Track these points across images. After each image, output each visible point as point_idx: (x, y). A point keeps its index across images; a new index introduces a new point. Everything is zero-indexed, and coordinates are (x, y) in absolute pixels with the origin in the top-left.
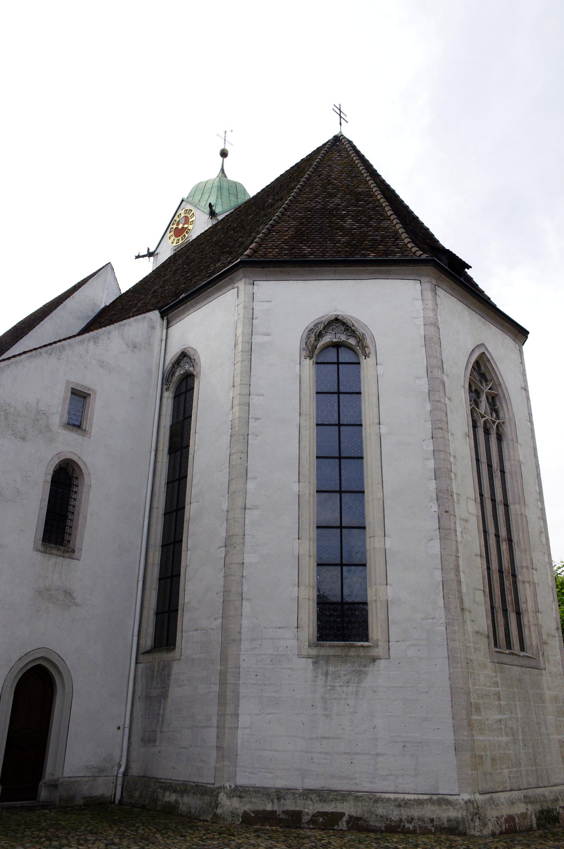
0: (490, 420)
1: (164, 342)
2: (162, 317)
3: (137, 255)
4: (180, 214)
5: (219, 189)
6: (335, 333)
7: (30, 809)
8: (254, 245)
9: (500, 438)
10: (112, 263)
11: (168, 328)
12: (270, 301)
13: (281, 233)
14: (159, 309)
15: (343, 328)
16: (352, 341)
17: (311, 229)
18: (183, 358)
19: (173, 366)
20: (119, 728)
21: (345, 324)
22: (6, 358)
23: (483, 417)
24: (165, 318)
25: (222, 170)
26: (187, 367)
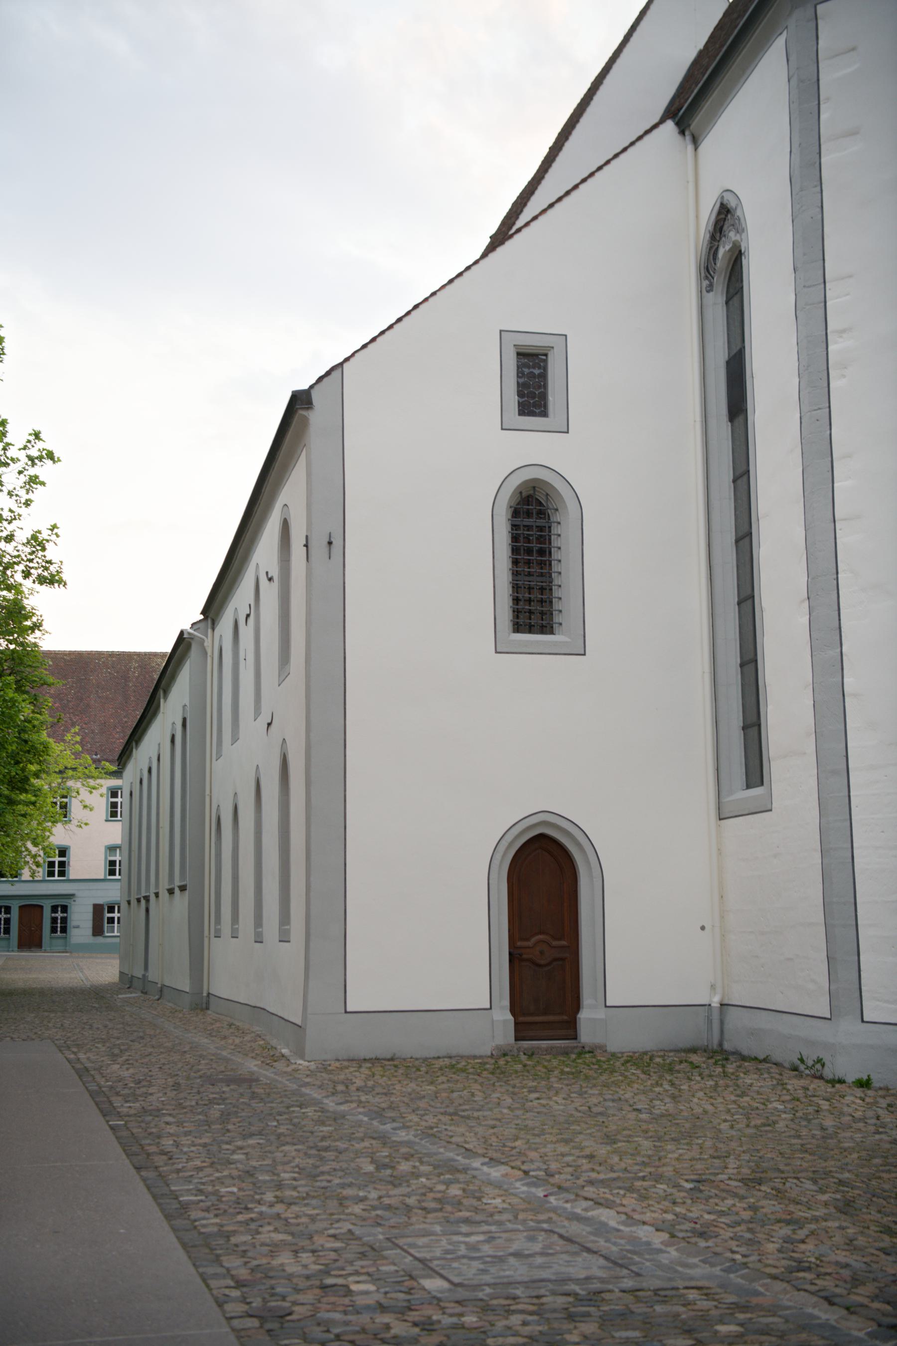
1: (691, 186)
2: (682, 132)
7: (566, 1053)
11: (696, 149)
18: (726, 216)
19: (713, 238)
22: (529, 219)
24: (687, 133)
26: (732, 235)
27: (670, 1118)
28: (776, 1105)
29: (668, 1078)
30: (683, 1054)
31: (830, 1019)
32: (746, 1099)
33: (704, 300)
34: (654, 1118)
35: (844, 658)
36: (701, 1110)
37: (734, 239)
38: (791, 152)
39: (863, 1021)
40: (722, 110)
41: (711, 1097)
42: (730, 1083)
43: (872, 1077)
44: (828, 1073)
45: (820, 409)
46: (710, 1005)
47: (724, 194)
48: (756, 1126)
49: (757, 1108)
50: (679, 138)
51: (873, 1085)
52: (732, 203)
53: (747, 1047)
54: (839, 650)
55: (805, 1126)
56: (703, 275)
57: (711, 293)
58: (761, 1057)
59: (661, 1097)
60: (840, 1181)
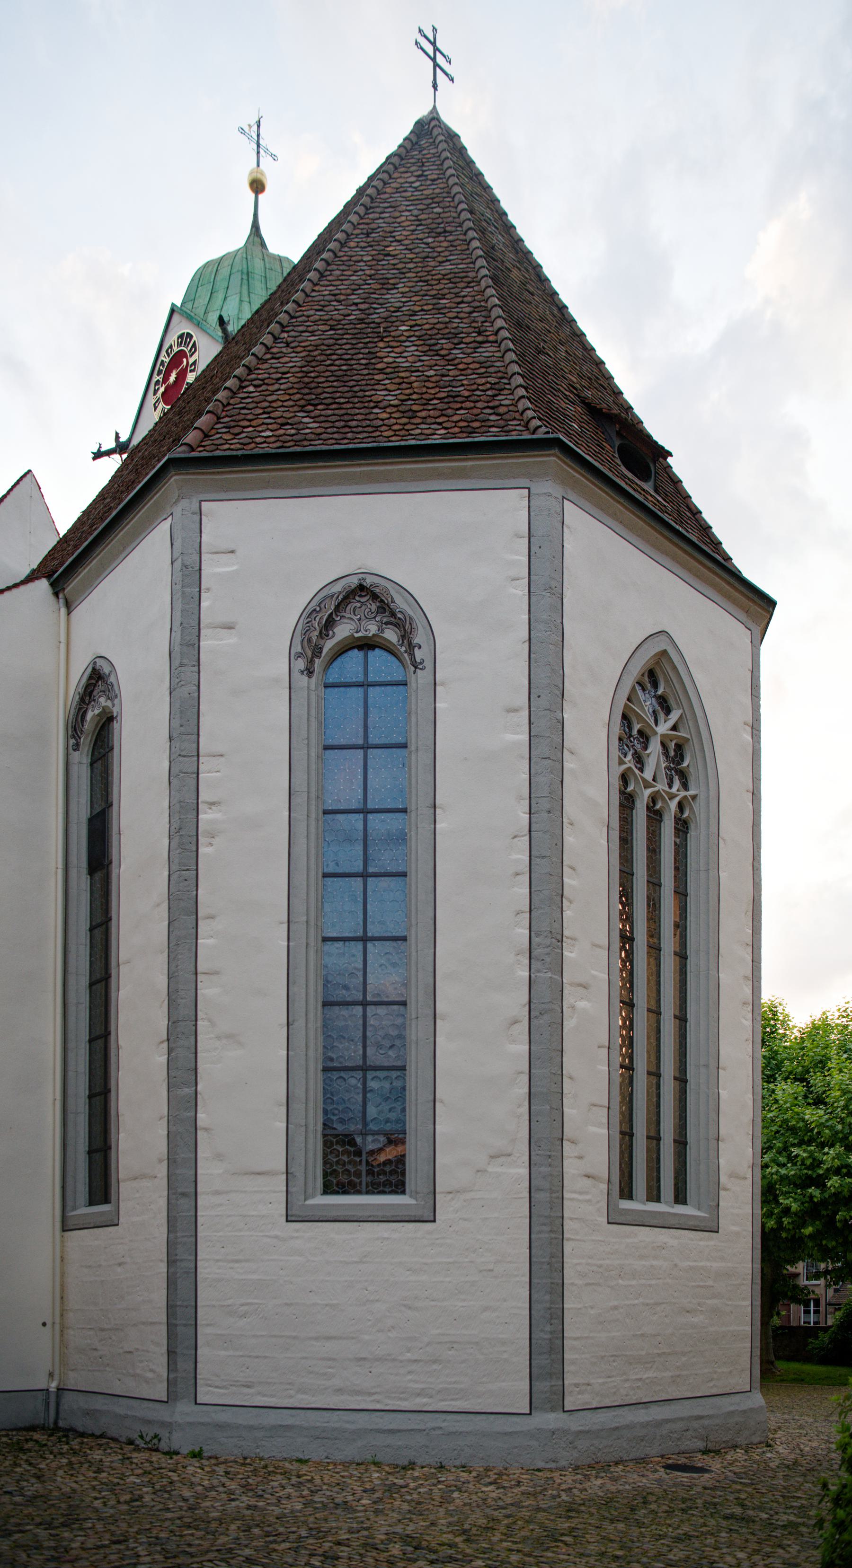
0: (664, 791)
1: (63, 647)
2: (56, 594)
3: (95, 451)
4: (171, 347)
5: (245, 277)
6: (359, 620)
8: (204, 418)
9: (682, 827)
10: (34, 472)
11: (69, 614)
12: (232, 552)
13: (264, 387)
14: (48, 576)
15: (374, 607)
16: (391, 635)
17: (328, 374)
18: (97, 682)
19: (82, 700)
20: (44, 1324)
21: (378, 597)
23: (647, 785)
24: (61, 596)
25: (255, 227)
26: (102, 700)
27: (43, 1499)
28: (132, 1479)
29: (25, 1457)
30: (25, 1433)
31: (167, 1402)
32: (104, 1475)
33: (70, 757)
34: (28, 1501)
35: (199, 1096)
36: (68, 1489)
37: (104, 704)
38: (171, 629)
39: (196, 1403)
40: (97, 582)
41: (72, 1475)
42: (82, 1460)
43: (204, 1448)
44: (163, 1446)
45: (188, 870)
46: (48, 1390)
47: (97, 660)
48: (126, 1502)
49: (118, 1484)
50: (52, 598)
51: (205, 1454)
52: (106, 669)
53: (90, 1426)
54: (194, 1088)
55: (168, 1499)
56: (70, 733)
57: (77, 752)
58: (98, 1433)
59: (25, 1478)
60: (247, 1558)
